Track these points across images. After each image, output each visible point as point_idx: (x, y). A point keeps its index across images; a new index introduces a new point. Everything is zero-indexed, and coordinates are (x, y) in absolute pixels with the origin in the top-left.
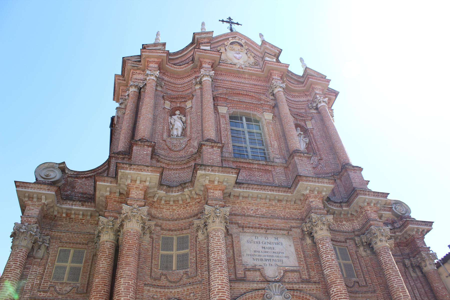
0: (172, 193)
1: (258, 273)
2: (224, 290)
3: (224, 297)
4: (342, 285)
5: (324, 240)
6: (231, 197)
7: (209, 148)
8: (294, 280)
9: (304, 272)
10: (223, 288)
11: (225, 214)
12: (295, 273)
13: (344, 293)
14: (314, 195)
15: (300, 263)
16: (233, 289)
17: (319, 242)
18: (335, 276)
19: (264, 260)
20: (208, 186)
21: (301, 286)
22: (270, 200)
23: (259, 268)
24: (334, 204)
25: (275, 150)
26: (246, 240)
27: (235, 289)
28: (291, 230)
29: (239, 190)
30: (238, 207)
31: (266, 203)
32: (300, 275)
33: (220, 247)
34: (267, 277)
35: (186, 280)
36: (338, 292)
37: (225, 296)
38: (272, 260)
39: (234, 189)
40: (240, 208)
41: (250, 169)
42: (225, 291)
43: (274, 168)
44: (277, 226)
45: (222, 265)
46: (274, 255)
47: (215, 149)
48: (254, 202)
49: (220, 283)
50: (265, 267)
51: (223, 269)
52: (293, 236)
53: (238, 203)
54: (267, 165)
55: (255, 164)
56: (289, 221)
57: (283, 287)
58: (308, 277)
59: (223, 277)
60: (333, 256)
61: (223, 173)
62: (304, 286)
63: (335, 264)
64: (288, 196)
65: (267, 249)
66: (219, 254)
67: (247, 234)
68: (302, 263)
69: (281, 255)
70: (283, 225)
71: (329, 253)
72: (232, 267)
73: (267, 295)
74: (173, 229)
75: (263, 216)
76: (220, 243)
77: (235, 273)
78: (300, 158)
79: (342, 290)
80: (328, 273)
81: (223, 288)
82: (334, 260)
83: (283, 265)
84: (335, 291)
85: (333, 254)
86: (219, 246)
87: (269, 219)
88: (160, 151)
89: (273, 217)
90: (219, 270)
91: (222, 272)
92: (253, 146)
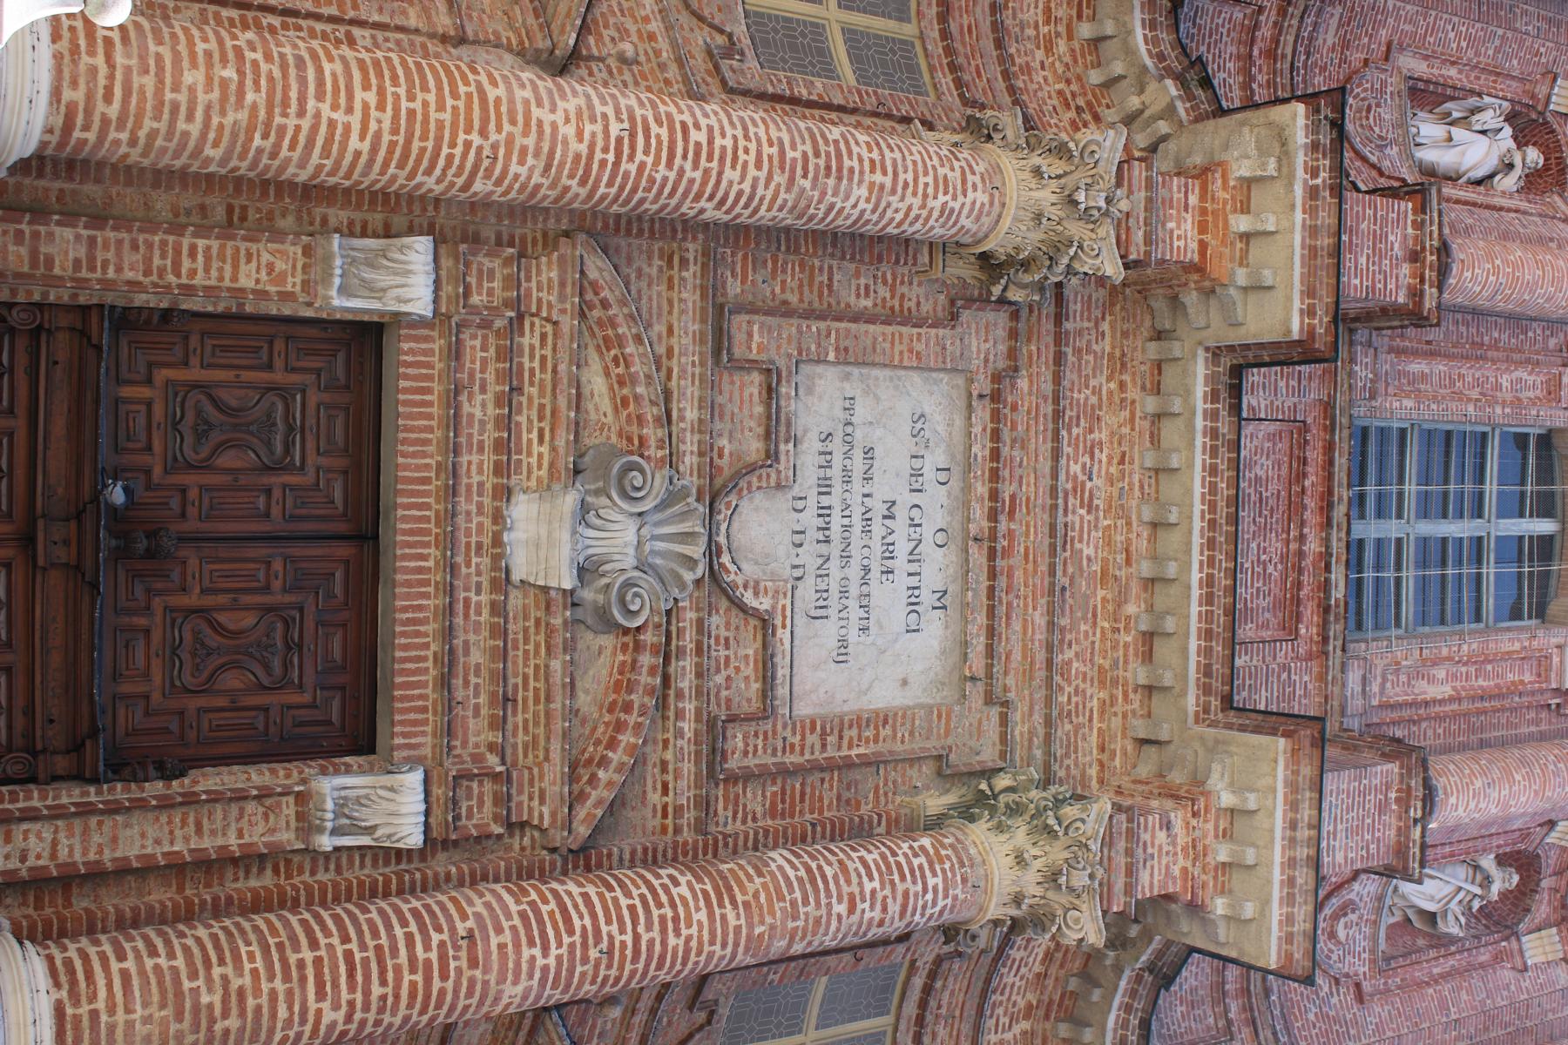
0: (1143, 20)
1: (753, 447)
2: (685, 157)
3: (646, 153)
4: (712, 943)
5: (962, 865)
6: (1153, 345)
7: (1405, 237)
8: (718, 671)
9: (760, 742)
10: (690, 155)
11: (1080, 247)
12: (756, 686)
13: (664, 943)
14: (1210, 840)
15: (813, 729)
16: (670, 279)
17: (946, 841)
18: (763, 899)
19: (825, 501)
20: (1218, 175)
21: (689, 706)
22: (1150, 583)
23: (783, 458)
24: (1134, 1022)
25: (1403, 678)
26: (927, 410)
27: (670, 287)
28: (989, 700)
29: (1200, 389)
30: (1097, 391)
31: (1128, 562)
32: (749, 718)
33: (906, 184)
34: (733, 498)
35: (701, 42)
36: (673, 905)
37: (650, 160)
38: (823, 549)
39: (1201, 353)
40: (1094, 400)
41: (1295, 508)
42: (678, 161)
43: (1310, 657)
44: (1008, 617)
45: (816, 178)
46: (854, 572)
47: (1406, 269)
48: (1131, 484)
49: (718, 142)
50: (782, 502)
51: (792, 180)
52: (957, 708)
53: (1122, 385)
54: (1327, 610)
55: (1327, 542)
56: (1037, 696)
57: (682, 586)
58: (733, 763)
59: (752, 172)
60: (872, 907)
61: (1303, 256)
62: (688, 727)
63: (829, 914)
64: (1184, 693)
65: (883, 532)
66: (873, 171)
67: (959, 422)
68: (813, 739)
69: (855, 613)
70: (1017, 656)
71: (892, 882)
72: (783, 291)
73: (642, 472)
74: (954, 27)
75: (1058, 538)
76: (930, 190)
77: (754, 310)
78: (1393, 795)
79: (684, 932)
80: (773, 866)
81: (690, 155)
82: (852, 909)
83: (800, 620)
84: (674, 891)
85: (884, 909)
86: (916, 180)
87: (1043, 568)
88: (1334, 22)
89: (1055, 595)
90: (790, 154)
91: (777, 170)
92: (1410, 552)
